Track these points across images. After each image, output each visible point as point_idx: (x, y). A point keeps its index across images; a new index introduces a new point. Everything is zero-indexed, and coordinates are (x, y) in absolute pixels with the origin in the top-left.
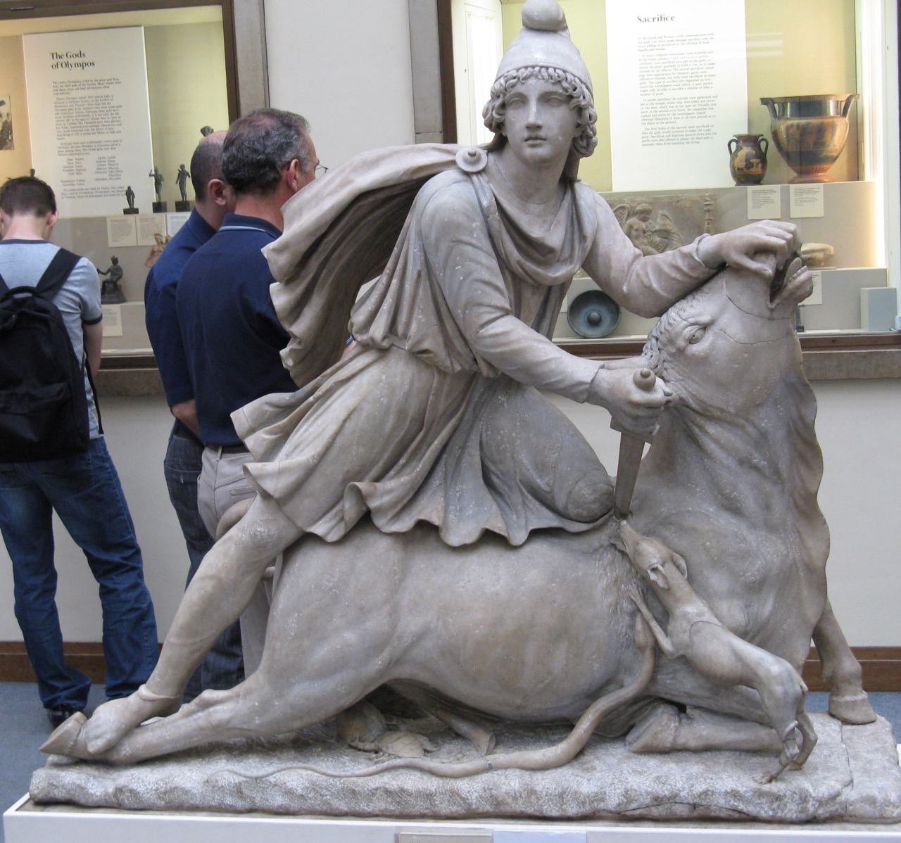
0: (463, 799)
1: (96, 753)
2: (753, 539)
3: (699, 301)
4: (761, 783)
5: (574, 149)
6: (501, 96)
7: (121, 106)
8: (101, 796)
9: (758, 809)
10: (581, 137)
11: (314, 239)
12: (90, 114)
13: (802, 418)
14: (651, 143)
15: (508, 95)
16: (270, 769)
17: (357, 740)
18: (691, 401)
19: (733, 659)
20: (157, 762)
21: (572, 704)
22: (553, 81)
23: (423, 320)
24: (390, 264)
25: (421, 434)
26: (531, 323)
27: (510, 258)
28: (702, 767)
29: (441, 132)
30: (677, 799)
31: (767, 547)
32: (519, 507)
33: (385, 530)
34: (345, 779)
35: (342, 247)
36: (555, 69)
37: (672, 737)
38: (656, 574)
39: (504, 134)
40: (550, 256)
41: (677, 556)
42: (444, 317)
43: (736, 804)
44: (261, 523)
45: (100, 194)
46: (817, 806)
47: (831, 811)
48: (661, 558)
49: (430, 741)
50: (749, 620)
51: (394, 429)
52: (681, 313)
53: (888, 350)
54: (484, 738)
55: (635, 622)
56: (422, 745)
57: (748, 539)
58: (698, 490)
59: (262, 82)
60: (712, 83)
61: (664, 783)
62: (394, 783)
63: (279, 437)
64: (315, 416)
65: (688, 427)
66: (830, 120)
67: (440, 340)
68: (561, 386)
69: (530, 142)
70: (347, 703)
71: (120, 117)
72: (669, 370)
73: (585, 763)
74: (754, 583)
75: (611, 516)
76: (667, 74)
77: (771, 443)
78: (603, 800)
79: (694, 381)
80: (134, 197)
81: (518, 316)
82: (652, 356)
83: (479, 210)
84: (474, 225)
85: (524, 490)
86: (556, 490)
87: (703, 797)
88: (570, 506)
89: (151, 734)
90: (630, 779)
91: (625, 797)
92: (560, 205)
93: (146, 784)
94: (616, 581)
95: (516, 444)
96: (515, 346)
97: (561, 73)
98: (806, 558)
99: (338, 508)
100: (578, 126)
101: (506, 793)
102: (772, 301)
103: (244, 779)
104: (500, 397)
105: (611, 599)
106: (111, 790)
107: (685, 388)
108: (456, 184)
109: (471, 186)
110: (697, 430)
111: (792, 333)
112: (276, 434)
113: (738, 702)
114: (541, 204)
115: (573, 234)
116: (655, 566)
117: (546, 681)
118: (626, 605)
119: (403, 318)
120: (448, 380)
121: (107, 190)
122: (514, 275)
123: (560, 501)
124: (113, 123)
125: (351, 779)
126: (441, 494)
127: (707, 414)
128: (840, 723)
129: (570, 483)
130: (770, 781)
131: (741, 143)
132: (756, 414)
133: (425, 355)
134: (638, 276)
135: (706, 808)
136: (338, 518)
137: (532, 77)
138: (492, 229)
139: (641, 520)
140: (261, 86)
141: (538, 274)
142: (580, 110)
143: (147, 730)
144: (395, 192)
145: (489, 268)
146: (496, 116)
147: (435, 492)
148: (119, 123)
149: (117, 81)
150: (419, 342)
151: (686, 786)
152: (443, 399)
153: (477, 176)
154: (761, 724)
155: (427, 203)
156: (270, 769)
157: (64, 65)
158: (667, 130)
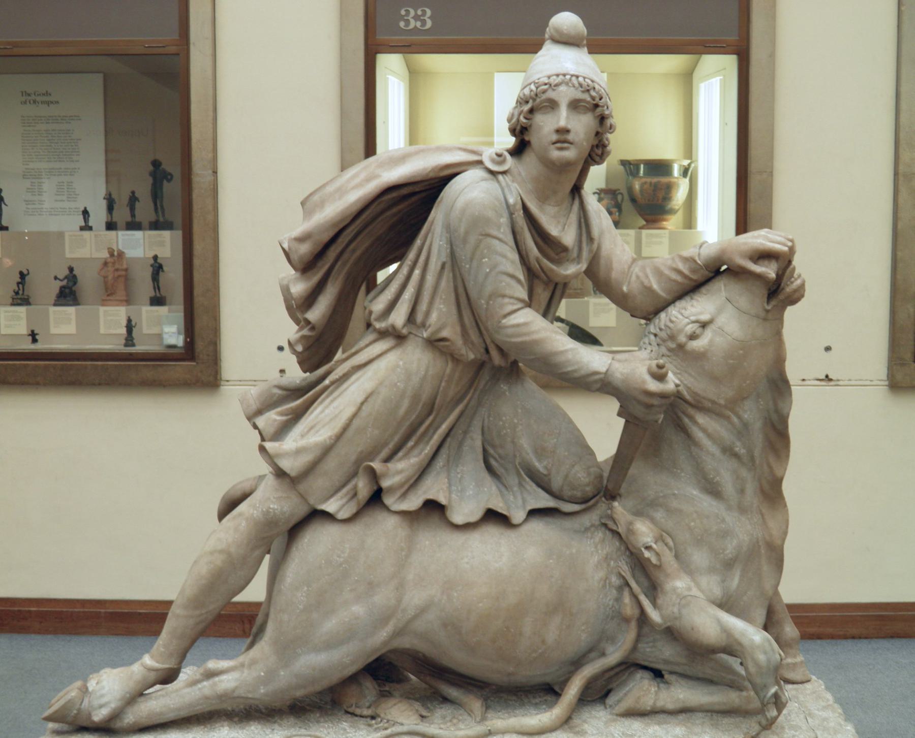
1: (101, 722)
2: (731, 519)
6: (531, 101)
7: (80, 140)
10: (597, 146)
11: (337, 230)
12: (52, 144)
13: (777, 411)
15: (538, 100)
17: (354, 706)
19: (718, 629)
20: (158, 729)
23: (444, 310)
24: (411, 255)
25: (431, 418)
28: (683, 728)
32: (515, 489)
35: (359, 238)
36: (584, 78)
37: (652, 701)
38: (649, 551)
39: (527, 138)
40: (563, 254)
42: (463, 308)
45: (58, 213)
49: (423, 706)
52: (683, 311)
54: (476, 705)
55: (622, 594)
56: (417, 711)
57: (727, 520)
58: (683, 474)
63: (290, 419)
64: (331, 398)
66: (676, 180)
67: (458, 329)
69: (559, 145)
73: (576, 727)
75: (601, 498)
79: (690, 375)
80: (89, 216)
83: (505, 206)
84: (502, 220)
85: (521, 470)
89: (155, 702)
94: (606, 558)
95: (517, 430)
96: (535, 337)
97: (590, 82)
102: (768, 303)
105: (601, 574)
108: (484, 182)
109: (497, 185)
110: (686, 420)
112: (287, 415)
114: (556, 206)
116: (649, 544)
117: (540, 651)
118: (615, 580)
119: (423, 307)
121: (65, 210)
123: (557, 482)
124: (73, 153)
127: (699, 406)
133: (442, 343)
134: (638, 277)
137: (563, 85)
141: (552, 270)
142: (602, 119)
143: (151, 698)
145: (513, 262)
148: (78, 153)
150: (440, 329)
153: (502, 175)
154: (731, 687)
155: (457, 198)
157: (32, 102)
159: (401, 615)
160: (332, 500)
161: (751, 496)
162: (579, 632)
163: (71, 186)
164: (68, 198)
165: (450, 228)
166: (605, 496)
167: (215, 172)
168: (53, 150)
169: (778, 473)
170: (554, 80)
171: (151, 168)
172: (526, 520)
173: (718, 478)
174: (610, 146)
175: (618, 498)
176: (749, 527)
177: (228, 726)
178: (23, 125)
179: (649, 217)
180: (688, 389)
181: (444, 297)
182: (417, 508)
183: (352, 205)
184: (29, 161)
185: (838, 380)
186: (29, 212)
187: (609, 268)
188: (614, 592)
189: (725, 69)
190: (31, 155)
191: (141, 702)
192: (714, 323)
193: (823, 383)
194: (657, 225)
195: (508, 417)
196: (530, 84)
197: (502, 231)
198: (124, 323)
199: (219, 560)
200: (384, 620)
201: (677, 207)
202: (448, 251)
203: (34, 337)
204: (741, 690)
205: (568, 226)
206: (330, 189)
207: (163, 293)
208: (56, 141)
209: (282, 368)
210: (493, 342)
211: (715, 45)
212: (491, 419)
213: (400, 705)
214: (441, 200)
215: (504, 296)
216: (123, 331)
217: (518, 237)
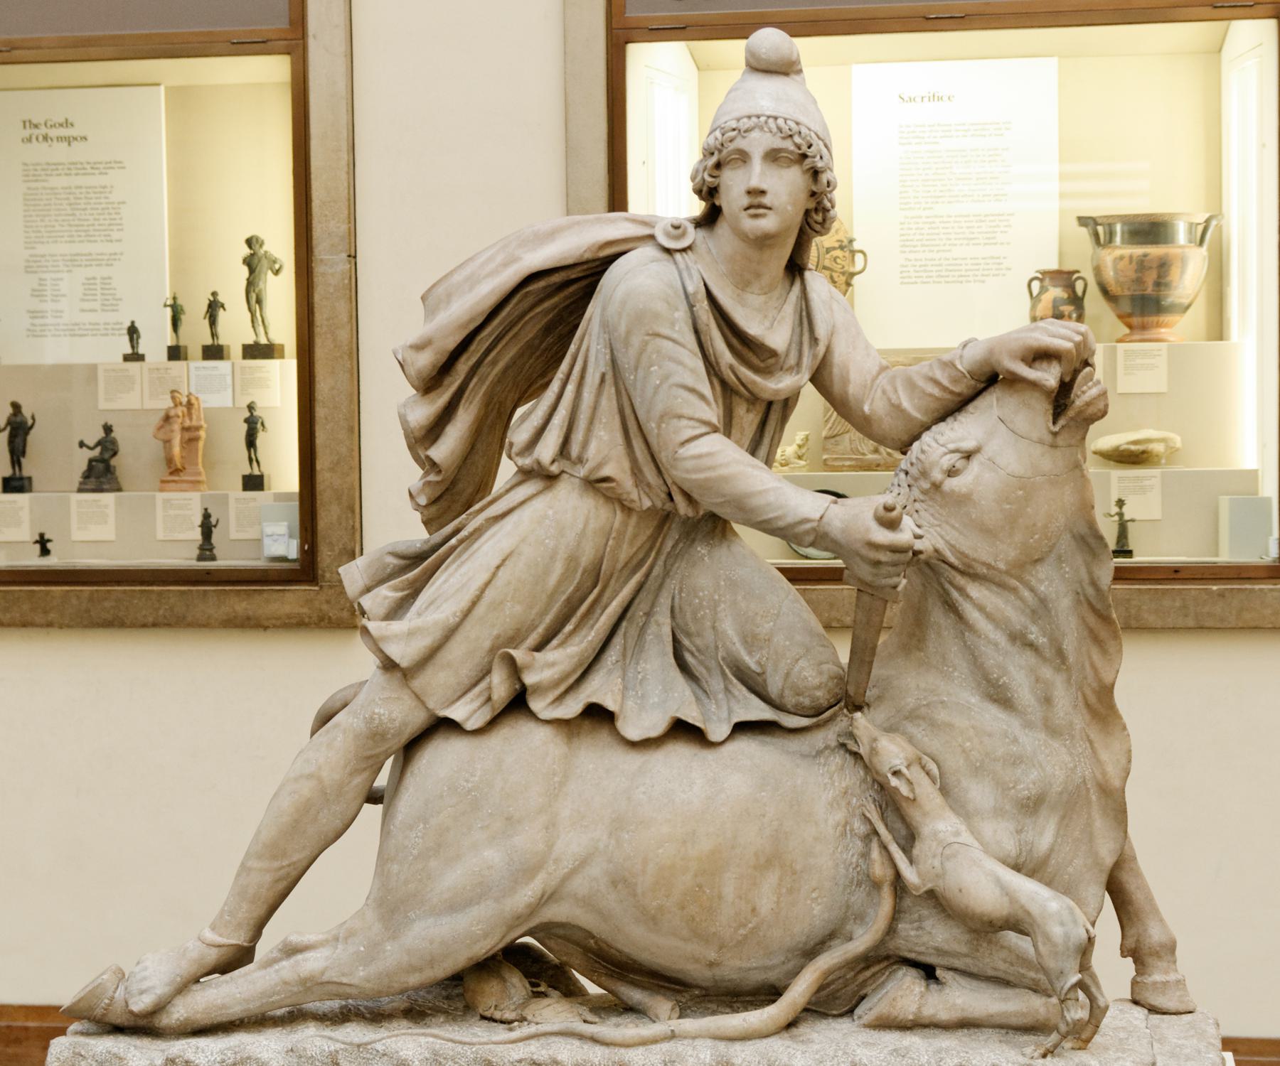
2: (1031, 741)
3: (962, 423)
4: (1032, 1058)
5: (807, 227)
6: (716, 153)
7: (124, 203)
10: (816, 210)
12: (77, 213)
14: (914, 280)
15: (725, 152)
16: (378, 1036)
17: (493, 1008)
19: (997, 891)
22: (783, 135)
23: (606, 438)
25: (596, 591)
26: (746, 446)
27: (720, 360)
32: (721, 696)
34: (477, 1046)
36: (786, 120)
37: (916, 1006)
39: (717, 203)
40: (771, 361)
42: (632, 435)
44: (379, 703)
45: (86, 332)
50: (1020, 849)
51: (560, 583)
52: (938, 437)
53: (1257, 587)
54: (663, 1005)
58: (956, 674)
59: (345, 169)
60: (1006, 195)
61: (903, 1056)
62: (544, 1052)
63: (407, 596)
64: (458, 562)
65: (944, 589)
66: (1179, 251)
67: (626, 464)
68: (781, 524)
69: (752, 211)
71: (121, 219)
72: (920, 513)
74: (1029, 798)
75: (841, 709)
77: (1053, 613)
79: (953, 527)
80: (138, 337)
81: (728, 433)
83: (683, 296)
84: (677, 315)
86: (769, 670)
88: (787, 692)
89: (215, 991)
90: (858, 1051)
92: (786, 298)
95: (719, 609)
97: (793, 125)
98: (1099, 777)
99: (483, 685)
100: (813, 194)
102: (1054, 423)
103: (343, 1046)
104: (699, 549)
105: (839, 816)
107: (942, 537)
109: (673, 267)
110: (955, 594)
111: (1081, 466)
112: (402, 590)
113: (1005, 961)
115: (801, 335)
117: (750, 925)
118: (860, 827)
119: (578, 437)
120: (634, 520)
121: (97, 327)
122: (724, 384)
123: (774, 686)
124: (112, 227)
125: (487, 1047)
126: (618, 673)
128: (1146, 1011)
129: (789, 661)
131: (1047, 282)
132: (1034, 573)
133: (605, 485)
136: (482, 699)
137: (756, 130)
138: (700, 322)
139: (880, 714)
140: (344, 176)
141: (754, 383)
142: (815, 173)
144: (573, 274)
145: (693, 371)
146: (708, 179)
147: (610, 672)
148: (120, 227)
149: (119, 165)
150: (599, 466)
154: (1035, 991)
155: (617, 285)
156: (378, 1036)
157: (41, 138)
158: (937, 262)
159: (553, 868)
160: (459, 703)
162: (809, 902)
163: (110, 284)
164: (103, 305)
165: (608, 327)
166: (846, 706)
167: (353, 257)
168: (77, 222)
170: (745, 124)
173: (1005, 678)
174: (837, 209)
176: (1067, 758)
177: (315, 1026)
178: (26, 178)
184: (35, 242)
186: (35, 331)
187: (845, 381)
188: (859, 844)
189: (1261, 45)
190: (39, 232)
191: (196, 991)
192: (982, 452)
194: (1148, 335)
195: (706, 593)
197: (677, 328)
198: (198, 520)
199: (306, 789)
200: (528, 871)
203: (43, 545)
205: (779, 322)
206: (457, 278)
207: (265, 469)
208: (83, 206)
212: (683, 595)
214: (601, 289)
215: (680, 417)
216: (197, 535)
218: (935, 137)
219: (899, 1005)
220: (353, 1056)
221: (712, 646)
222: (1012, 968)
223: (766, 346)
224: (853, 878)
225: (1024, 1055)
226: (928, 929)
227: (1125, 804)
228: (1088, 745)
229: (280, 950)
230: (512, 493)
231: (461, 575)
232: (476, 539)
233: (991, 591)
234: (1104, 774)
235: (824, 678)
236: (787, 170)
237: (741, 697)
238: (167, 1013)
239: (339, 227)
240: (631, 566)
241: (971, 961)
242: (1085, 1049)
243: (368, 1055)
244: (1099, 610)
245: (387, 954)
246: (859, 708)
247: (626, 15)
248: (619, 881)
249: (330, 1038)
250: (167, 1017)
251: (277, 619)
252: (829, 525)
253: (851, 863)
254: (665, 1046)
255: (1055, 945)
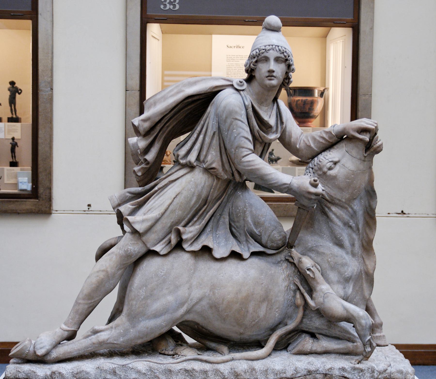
0: (222, 373)
2: (348, 258)
4: (355, 364)
6: (256, 57)
8: (43, 376)
9: (353, 376)
11: (162, 116)
13: (370, 206)
15: (260, 57)
18: (326, 196)
19: (342, 309)
21: (264, 333)
22: (281, 52)
23: (214, 154)
24: (199, 129)
25: (205, 207)
27: (254, 128)
29: (139, 91)
30: (318, 372)
31: (352, 263)
32: (244, 243)
33: (188, 249)
34: (166, 365)
35: (171, 121)
36: (281, 47)
37: (311, 347)
39: (253, 74)
41: (317, 265)
42: (222, 153)
43: (344, 374)
44: (130, 245)
46: (378, 374)
47: (384, 377)
48: (312, 264)
51: (195, 203)
52: (326, 157)
54: (225, 349)
61: (312, 365)
62: (189, 366)
63: (137, 207)
65: (322, 208)
66: (316, 99)
67: (220, 163)
69: (269, 78)
70: (165, 331)
75: (285, 247)
76: (239, 73)
78: (285, 373)
79: (329, 187)
82: (311, 176)
86: (263, 234)
87: (330, 370)
88: (269, 242)
89: (67, 347)
91: (295, 371)
92: (273, 108)
93: (67, 370)
96: (257, 167)
97: (284, 49)
98: (366, 270)
101: (241, 370)
102: (365, 153)
103: (117, 366)
104: (238, 193)
105: (286, 284)
106: (49, 373)
108: (234, 94)
109: (240, 96)
110: (327, 209)
113: (339, 331)
116: (309, 268)
117: (256, 321)
118: (293, 287)
119: (204, 153)
120: (220, 183)
123: (264, 239)
127: (333, 202)
130: (358, 363)
132: (353, 202)
133: (212, 170)
134: (304, 141)
135: (331, 376)
137: (271, 50)
139: (300, 249)
141: (264, 136)
142: (289, 66)
145: (247, 132)
147: (208, 234)
150: (212, 164)
151: (322, 366)
152: (216, 191)
154: (349, 341)
155: (221, 102)
160: (158, 245)
161: (357, 248)
162: (275, 312)
166: (287, 246)
169: (371, 237)
170: (268, 48)
171: (9, 86)
172: (249, 257)
174: (292, 78)
175: (294, 247)
179: (301, 120)
180: (328, 194)
181: (214, 148)
182: (199, 249)
183: (171, 104)
185: (409, 214)
187: (290, 137)
188: (292, 292)
189: (345, 35)
191: (60, 347)
193: (400, 215)
196: (256, 49)
197: (243, 117)
201: (317, 115)
202: (217, 126)
204: (353, 343)
205: (272, 116)
207: (17, 160)
209: (89, 203)
210: (237, 170)
211: (340, 22)
213: (187, 349)
215: (243, 147)
217: (249, 121)
218: (238, 59)
219: (305, 347)
220: (121, 369)
221: (243, 226)
222: (341, 333)
223: (269, 124)
224: (289, 304)
225: (352, 363)
226: (314, 321)
227: (374, 278)
228: (362, 259)
229: (91, 332)
230: (178, 172)
231: (160, 201)
232: (165, 188)
233: (338, 208)
234: (367, 269)
235: (281, 237)
236: (281, 64)
237: (252, 243)
238: (50, 355)
239: (48, 79)
240: (217, 198)
241: (328, 332)
242: (367, 360)
243: (126, 369)
244: (371, 215)
245: (131, 333)
246: (292, 247)
247: (147, 14)
248: (214, 306)
249: (113, 363)
250: (49, 357)
251: (24, 210)
252: (293, 186)
253: (289, 299)
254: (230, 363)
255: (362, 326)
